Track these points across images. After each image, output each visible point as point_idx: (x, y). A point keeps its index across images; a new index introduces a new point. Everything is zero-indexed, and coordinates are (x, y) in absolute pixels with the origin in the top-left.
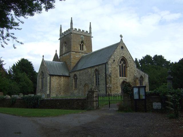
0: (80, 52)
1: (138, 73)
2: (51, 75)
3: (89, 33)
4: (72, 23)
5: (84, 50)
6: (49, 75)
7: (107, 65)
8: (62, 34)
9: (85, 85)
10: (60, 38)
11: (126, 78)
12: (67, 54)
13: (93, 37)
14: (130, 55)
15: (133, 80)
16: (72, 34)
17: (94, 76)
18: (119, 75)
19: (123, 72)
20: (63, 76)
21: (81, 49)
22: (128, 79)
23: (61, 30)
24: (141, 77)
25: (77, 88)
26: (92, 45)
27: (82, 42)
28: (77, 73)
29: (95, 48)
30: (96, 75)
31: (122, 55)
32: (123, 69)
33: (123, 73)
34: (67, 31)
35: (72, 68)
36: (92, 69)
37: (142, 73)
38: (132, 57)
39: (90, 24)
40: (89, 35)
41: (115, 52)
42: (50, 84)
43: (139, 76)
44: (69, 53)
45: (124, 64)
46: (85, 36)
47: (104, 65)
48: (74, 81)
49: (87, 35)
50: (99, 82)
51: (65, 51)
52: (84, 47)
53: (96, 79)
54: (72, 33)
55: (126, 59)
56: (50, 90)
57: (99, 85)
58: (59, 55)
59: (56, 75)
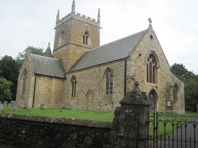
0: (83, 46)
1: (172, 79)
2: (37, 75)
3: (96, 21)
4: (73, 6)
5: (88, 44)
6: (35, 74)
7: (127, 61)
8: (60, 21)
9: (88, 93)
10: (55, 26)
12: (64, 48)
13: (101, 28)
14: (162, 50)
15: (165, 90)
16: (73, 20)
18: (146, 80)
19: (151, 75)
20: (56, 78)
21: (84, 43)
23: (58, 15)
24: (176, 86)
25: (75, 96)
26: (99, 39)
27: (87, 33)
28: (77, 75)
29: (103, 42)
30: (107, 77)
33: (151, 77)
34: (65, 16)
35: (69, 68)
37: (176, 79)
38: (164, 54)
39: (99, 11)
40: (97, 25)
41: (141, 42)
42: (35, 88)
43: (173, 84)
44: (67, 46)
47: (123, 63)
48: (71, 85)
49: (94, 24)
50: (112, 88)
51: (61, 44)
52: (89, 40)
53: (108, 84)
54: (72, 19)
57: (111, 93)
58: (52, 50)
59: (44, 76)
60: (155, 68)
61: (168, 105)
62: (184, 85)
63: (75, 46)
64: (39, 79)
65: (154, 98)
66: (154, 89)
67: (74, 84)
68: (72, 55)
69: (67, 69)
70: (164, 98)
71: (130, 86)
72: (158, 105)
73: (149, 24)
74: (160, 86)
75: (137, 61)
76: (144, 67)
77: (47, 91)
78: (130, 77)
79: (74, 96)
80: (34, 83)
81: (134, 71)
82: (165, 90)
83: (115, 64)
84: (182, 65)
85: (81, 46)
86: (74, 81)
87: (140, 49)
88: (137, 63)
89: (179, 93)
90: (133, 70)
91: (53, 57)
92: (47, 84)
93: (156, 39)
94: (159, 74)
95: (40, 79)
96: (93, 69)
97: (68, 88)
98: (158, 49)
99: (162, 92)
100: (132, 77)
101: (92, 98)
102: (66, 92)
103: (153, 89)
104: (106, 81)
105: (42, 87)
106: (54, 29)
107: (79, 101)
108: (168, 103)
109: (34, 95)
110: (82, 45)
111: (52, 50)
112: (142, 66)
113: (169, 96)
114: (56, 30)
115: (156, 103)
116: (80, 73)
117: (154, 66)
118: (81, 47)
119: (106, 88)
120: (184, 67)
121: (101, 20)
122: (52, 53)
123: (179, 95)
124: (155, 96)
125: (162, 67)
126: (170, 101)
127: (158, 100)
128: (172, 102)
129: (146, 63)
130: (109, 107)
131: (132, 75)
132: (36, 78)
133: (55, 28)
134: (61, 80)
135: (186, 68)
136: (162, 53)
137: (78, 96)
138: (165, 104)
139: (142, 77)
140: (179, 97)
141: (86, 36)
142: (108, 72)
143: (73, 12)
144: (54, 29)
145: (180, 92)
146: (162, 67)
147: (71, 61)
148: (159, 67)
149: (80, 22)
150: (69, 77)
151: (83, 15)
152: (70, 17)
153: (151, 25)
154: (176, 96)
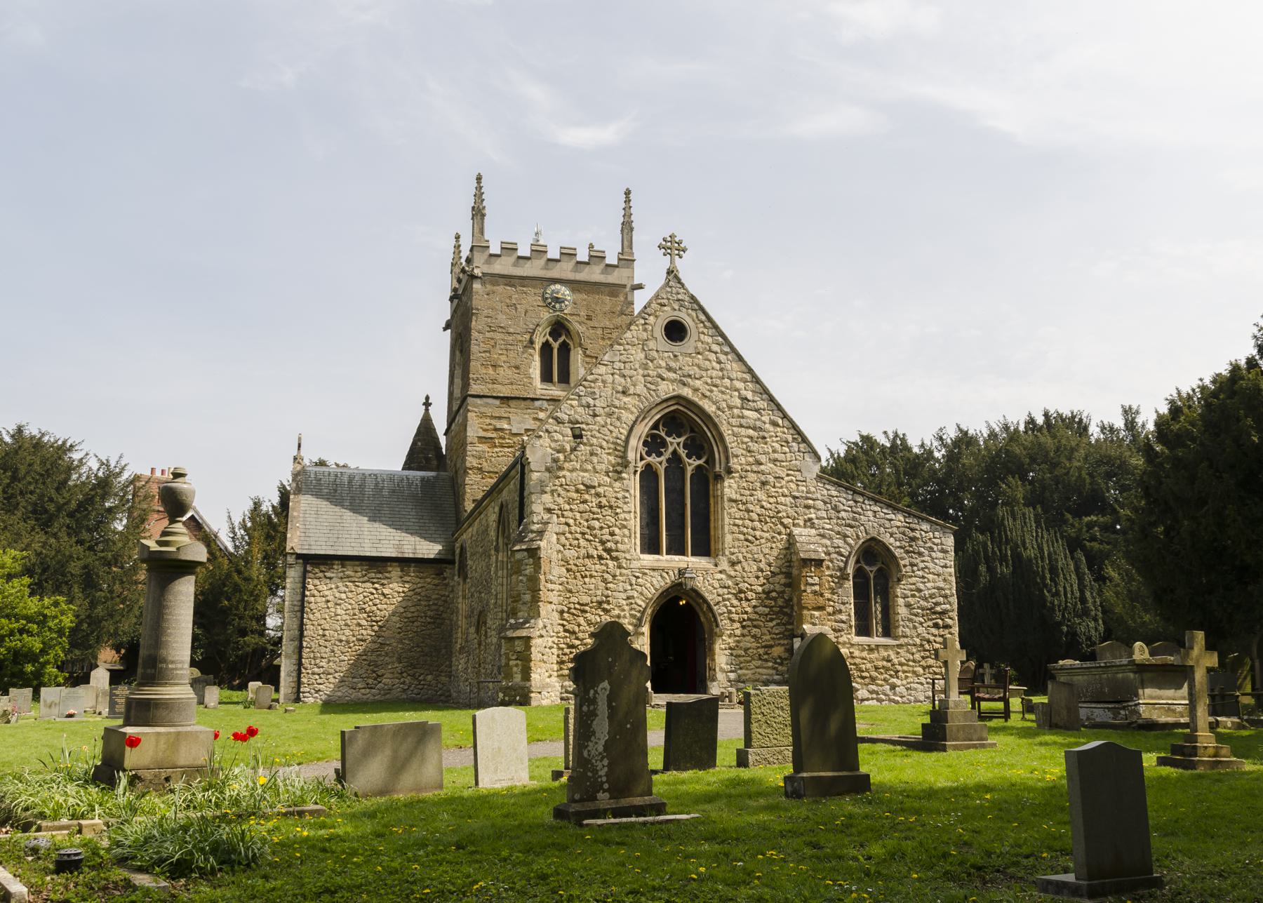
3: (612, 259)
4: (478, 213)
18: (631, 542)
21: (546, 377)
27: (559, 328)
60: (711, 481)
63: (497, 402)
64: (321, 575)
70: (771, 624)
77: (364, 622)
95: (328, 574)
106: (445, 329)
117: (699, 467)
118: (528, 401)
122: (443, 441)
132: (305, 572)
141: (556, 346)
144: (445, 329)
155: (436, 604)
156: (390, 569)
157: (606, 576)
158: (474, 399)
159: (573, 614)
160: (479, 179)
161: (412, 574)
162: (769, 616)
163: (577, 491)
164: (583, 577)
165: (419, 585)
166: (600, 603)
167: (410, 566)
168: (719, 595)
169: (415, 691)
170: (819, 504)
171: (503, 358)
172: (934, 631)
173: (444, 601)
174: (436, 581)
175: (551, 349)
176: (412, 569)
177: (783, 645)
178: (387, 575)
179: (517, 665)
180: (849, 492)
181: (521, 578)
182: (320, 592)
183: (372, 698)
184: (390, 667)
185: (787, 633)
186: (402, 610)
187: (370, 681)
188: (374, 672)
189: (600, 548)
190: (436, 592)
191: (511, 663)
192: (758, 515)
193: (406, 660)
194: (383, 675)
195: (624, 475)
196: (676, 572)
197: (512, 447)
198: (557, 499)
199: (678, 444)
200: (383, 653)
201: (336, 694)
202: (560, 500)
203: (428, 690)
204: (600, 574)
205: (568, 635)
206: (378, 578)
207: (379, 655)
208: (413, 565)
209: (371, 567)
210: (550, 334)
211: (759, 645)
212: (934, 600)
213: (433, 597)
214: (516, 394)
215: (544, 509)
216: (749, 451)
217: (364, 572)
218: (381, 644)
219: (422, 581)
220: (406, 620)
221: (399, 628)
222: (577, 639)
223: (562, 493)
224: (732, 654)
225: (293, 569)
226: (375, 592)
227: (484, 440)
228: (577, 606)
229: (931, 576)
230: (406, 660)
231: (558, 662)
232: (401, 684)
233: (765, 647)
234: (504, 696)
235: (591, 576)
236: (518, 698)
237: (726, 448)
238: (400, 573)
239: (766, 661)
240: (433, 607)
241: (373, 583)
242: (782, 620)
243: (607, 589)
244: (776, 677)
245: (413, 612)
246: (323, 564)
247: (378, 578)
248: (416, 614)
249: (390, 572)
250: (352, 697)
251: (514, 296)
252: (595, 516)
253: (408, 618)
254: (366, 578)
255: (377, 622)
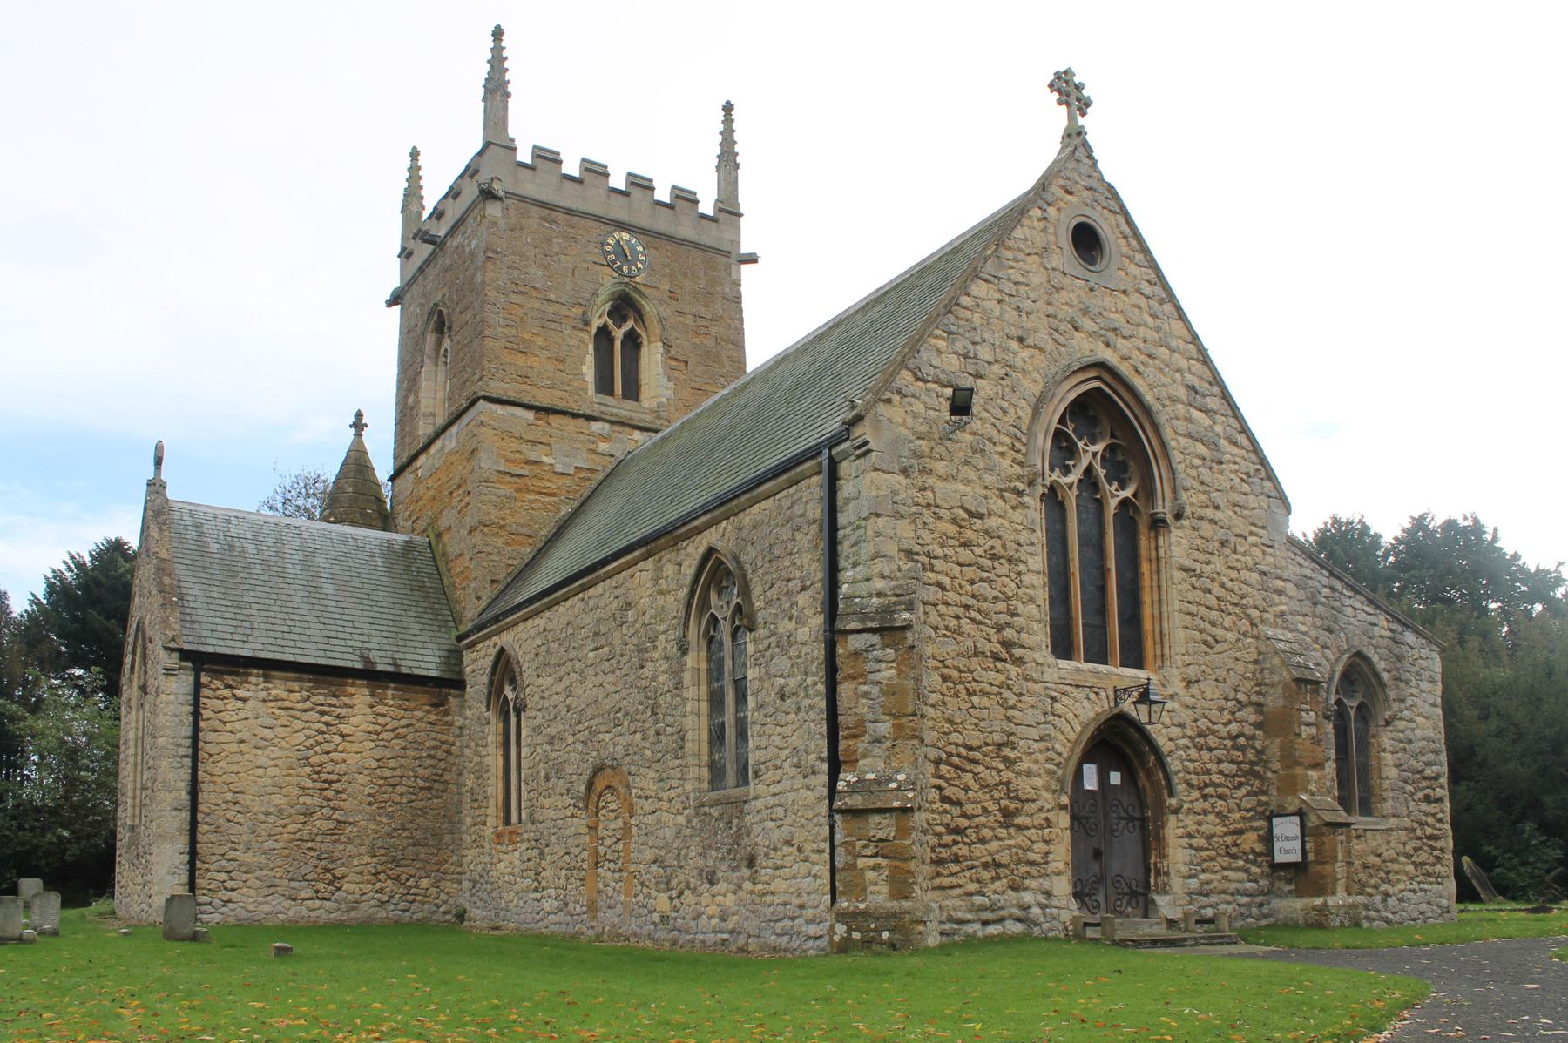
0: (596, 410)
3: (707, 206)
4: (496, 89)
6: (185, 655)
7: (845, 468)
9: (590, 786)
10: (396, 283)
11: (1141, 674)
12: (450, 441)
13: (752, 259)
14: (1206, 360)
17: (690, 660)
18: (1038, 635)
19: (1102, 589)
20: (371, 676)
21: (605, 386)
22: (1177, 686)
27: (624, 305)
31: (1086, 347)
32: (1101, 551)
36: (669, 569)
38: (1226, 396)
39: (728, 121)
40: (709, 236)
43: (1325, 664)
44: (465, 419)
45: (1118, 474)
46: (659, 235)
47: (814, 486)
48: (493, 732)
49: (686, 231)
52: (652, 359)
53: (716, 701)
55: (1147, 410)
56: (193, 842)
58: (383, 467)
60: (1143, 528)
61: (1277, 845)
62: (1437, 666)
63: (530, 415)
64: (226, 692)
65: (1139, 794)
66: (1127, 706)
67: (513, 720)
68: (506, 490)
69: (471, 611)
71: (865, 695)
72: (1178, 856)
73: (1065, 123)
74: (1189, 683)
75: (940, 467)
76: (1017, 516)
77: (309, 784)
78: (865, 616)
79: (514, 819)
80: (187, 731)
81: (910, 554)
82: (1253, 718)
83: (755, 509)
84: (1477, 528)
85: (575, 416)
86: (510, 695)
87: (960, 346)
88: (930, 481)
89: (1386, 739)
90: (891, 549)
91: (385, 521)
92: (300, 731)
93: (1139, 257)
94: (1178, 575)
95: (240, 693)
96: (612, 582)
97: (476, 759)
98: (1163, 352)
99: (1212, 740)
100: (886, 611)
101: (620, 823)
102: (469, 784)
103: (1122, 717)
104: (704, 675)
105: (263, 761)
106: (390, 304)
107: (542, 855)
108: (1276, 831)
109: (194, 823)
110: (590, 399)
111: (383, 467)
112: (997, 504)
113: (1285, 767)
114: (402, 309)
115: (1160, 841)
116: (540, 622)
117: (1125, 503)
118: (581, 421)
119: (705, 736)
120: (1495, 539)
121: (746, 199)
122: (387, 490)
123: (1388, 758)
124: (1143, 781)
125: (1209, 513)
126: (1300, 813)
127: (1176, 811)
128: (1313, 821)
129: (1031, 483)
130: (730, 901)
131: (879, 595)
132: (198, 686)
133: (395, 300)
134: (421, 699)
135: (1507, 545)
136: (1203, 387)
137: (537, 816)
138: (1250, 841)
139: (1001, 606)
140: (1392, 773)
141: (619, 334)
142: (713, 596)
143: (496, 141)
144: (390, 304)
145: (1401, 725)
146: (1209, 513)
147: (500, 542)
148: (1178, 516)
149: (561, 217)
150: (477, 664)
151: (535, 147)
152: (471, 192)
153: (1080, 133)
154: (1365, 772)
155: (432, 757)
156: (351, 690)
157: (1006, 693)
158: (492, 405)
159: (957, 767)
160: (498, 33)
161: (391, 702)
162: (1237, 779)
163: (954, 521)
164: (969, 694)
165: (404, 722)
166: (1000, 745)
167: (387, 688)
168: (1171, 740)
169: (401, 906)
170: (1290, 589)
171: (540, 341)
172: (1424, 806)
173: (446, 752)
174: (433, 717)
175: (612, 341)
176: (390, 693)
177: (1256, 829)
178: (347, 700)
179: (875, 868)
180: (1324, 572)
181: (864, 688)
182: (225, 723)
183: (324, 916)
184: (355, 862)
185: (1260, 809)
186: (374, 764)
187: (321, 886)
188: (328, 870)
189: (995, 638)
190: (433, 735)
191: (861, 862)
192: (1218, 598)
193: (384, 852)
194: (342, 878)
195: (1026, 499)
196: (1111, 694)
197: (553, 495)
198: (921, 532)
199: (1095, 454)
200: (343, 838)
201: (261, 907)
202: (925, 534)
203: (423, 903)
204: (995, 689)
205: (947, 806)
206: (330, 705)
207: (335, 841)
208: (392, 685)
209: (318, 684)
210: (609, 314)
211: (1226, 829)
212: (1424, 758)
213: (427, 744)
214: (560, 405)
215: (900, 550)
216: (1202, 483)
217: (305, 694)
218: (339, 822)
219: (408, 714)
220: (381, 782)
221: (370, 795)
222: (964, 815)
223: (930, 520)
224: (1191, 846)
225: (174, 678)
226: (324, 728)
227: (508, 478)
228: (963, 751)
229: (1419, 719)
230: (384, 852)
231: (932, 861)
232: (377, 892)
233: (1233, 833)
234: (849, 930)
235: (984, 693)
236: (886, 935)
237: (1173, 472)
238: (369, 699)
239: (1234, 857)
240: (429, 762)
241: (323, 713)
242: (1252, 785)
243: (1008, 719)
244: (1249, 885)
245: (393, 769)
246: (230, 673)
247: (330, 705)
248: (398, 772)
249: (352, 695)
250: (291, 913)
251: (555, 240)
252: (985, 575)
253: (386, 778)
254: (308, 704)
255: (331, 782)
